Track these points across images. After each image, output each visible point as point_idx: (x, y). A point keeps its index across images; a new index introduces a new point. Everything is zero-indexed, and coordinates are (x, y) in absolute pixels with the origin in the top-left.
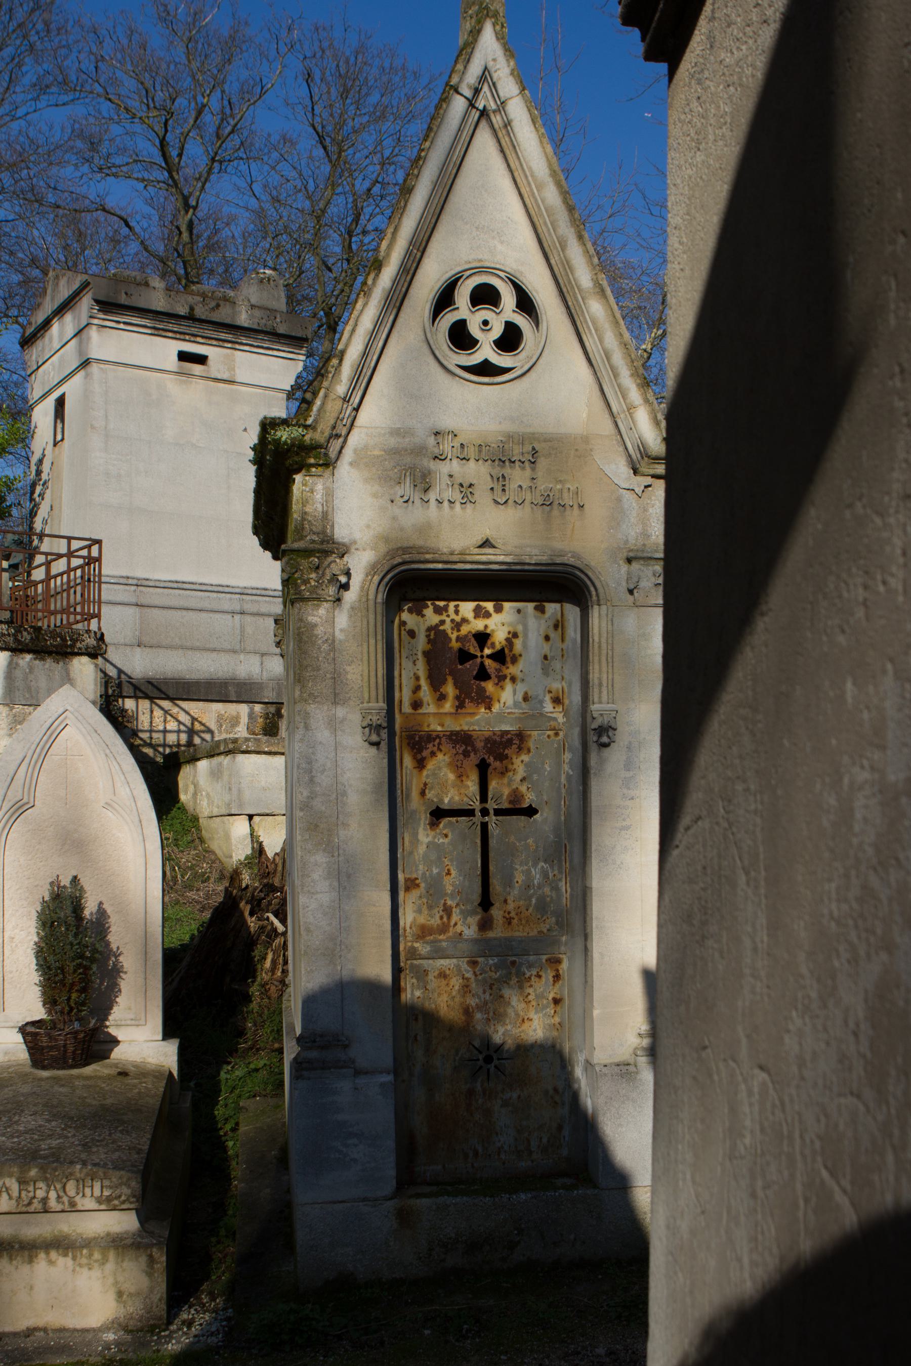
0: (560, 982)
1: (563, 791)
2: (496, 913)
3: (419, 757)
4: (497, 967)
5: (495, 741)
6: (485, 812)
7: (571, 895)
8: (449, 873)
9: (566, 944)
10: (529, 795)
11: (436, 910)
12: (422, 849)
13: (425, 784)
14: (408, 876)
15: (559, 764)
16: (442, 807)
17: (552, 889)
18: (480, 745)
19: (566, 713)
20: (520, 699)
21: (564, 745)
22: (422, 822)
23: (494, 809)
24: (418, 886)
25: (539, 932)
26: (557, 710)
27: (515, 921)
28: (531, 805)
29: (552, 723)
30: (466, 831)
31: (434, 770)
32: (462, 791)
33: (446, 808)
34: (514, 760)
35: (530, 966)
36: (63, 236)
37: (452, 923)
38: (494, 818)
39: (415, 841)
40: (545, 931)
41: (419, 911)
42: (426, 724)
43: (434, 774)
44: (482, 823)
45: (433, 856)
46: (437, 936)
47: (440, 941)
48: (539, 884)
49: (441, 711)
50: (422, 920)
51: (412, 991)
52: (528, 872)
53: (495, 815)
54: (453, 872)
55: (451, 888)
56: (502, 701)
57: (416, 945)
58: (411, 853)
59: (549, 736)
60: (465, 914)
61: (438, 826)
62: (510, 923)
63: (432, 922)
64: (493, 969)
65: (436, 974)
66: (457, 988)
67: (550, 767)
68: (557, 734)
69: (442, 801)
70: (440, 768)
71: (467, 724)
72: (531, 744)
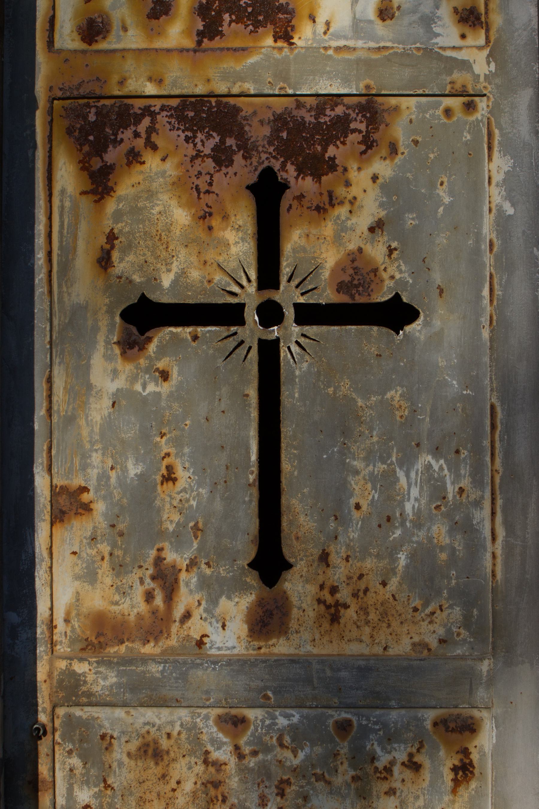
0: (473, 785)
1: (488, 259)
2: (298, 587)
3: (96, 164)
4: (297, 736)
5: (301, 125)
6: (270, 314)
7: (508, 548)
8: (170, 477)
9: (491, 681)
10: (392, 270)
11: (134, 577)
12: (99, 410)
13: (112, 237)
14: (59, 481)
15: (475, 188)
16: (155, 297)
17: (454, 527)
18: (259, 132)
19: (495, 51)
20: (371, 14)
21: (490, 135)
22: (101, 338)
23: (297, 306)
24: (87, 508)
25: (414, 645)
26: (470, 41)
27: (350, 614)
28: (397, 296)
29: (459, 77)
30: (220, 362)
31: (137, 198)
32: (211, 255)
33: (166, 299)
34: (353, 174)
35: (390, 738)
36: (378, 778)
37: (178, 612)
38: (296, 329)
39: (82, 389)
40: (434, 643)
41: (90, 576)
42: (115, 78)
43: (136, 211)
44: (262, 343)
45: (129, 431)
46: (137, 645)
47: (145, 660)
48: (418, 513)
49: (159, 44)
50: (97, 600)
51: (70, 790)
52: (387, 482)
53: (299, 321)
54: (183, 475)
55: (176, 517)
56: (321, 19)
57: (80, 668)
58: (70, 420)
59: (448, 112)
60: (213, 589)
61: (142, 348)
62: (335, 619)
63: (125, 606)
64: (287, 739)
65: (133, 746)
66: (188, 786)
67: (451, 193)
68: (470, 107)
69: (154, 280)
70: (151, 195)
71: (225, 76)
72: (400, 131)
